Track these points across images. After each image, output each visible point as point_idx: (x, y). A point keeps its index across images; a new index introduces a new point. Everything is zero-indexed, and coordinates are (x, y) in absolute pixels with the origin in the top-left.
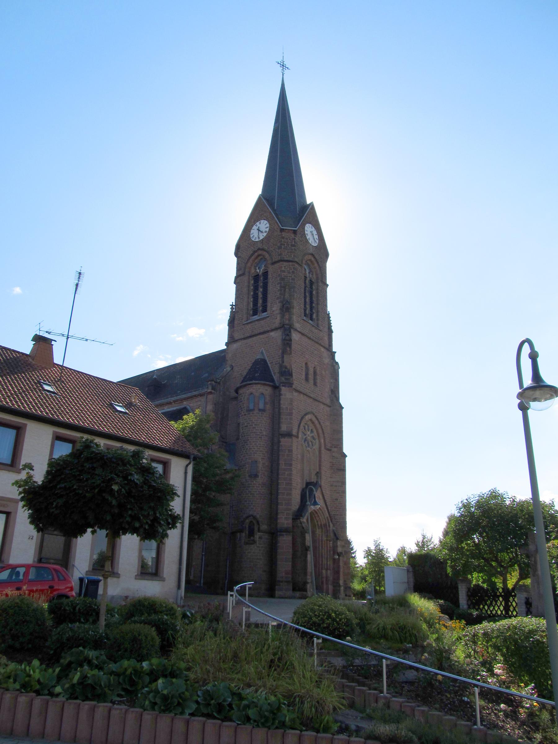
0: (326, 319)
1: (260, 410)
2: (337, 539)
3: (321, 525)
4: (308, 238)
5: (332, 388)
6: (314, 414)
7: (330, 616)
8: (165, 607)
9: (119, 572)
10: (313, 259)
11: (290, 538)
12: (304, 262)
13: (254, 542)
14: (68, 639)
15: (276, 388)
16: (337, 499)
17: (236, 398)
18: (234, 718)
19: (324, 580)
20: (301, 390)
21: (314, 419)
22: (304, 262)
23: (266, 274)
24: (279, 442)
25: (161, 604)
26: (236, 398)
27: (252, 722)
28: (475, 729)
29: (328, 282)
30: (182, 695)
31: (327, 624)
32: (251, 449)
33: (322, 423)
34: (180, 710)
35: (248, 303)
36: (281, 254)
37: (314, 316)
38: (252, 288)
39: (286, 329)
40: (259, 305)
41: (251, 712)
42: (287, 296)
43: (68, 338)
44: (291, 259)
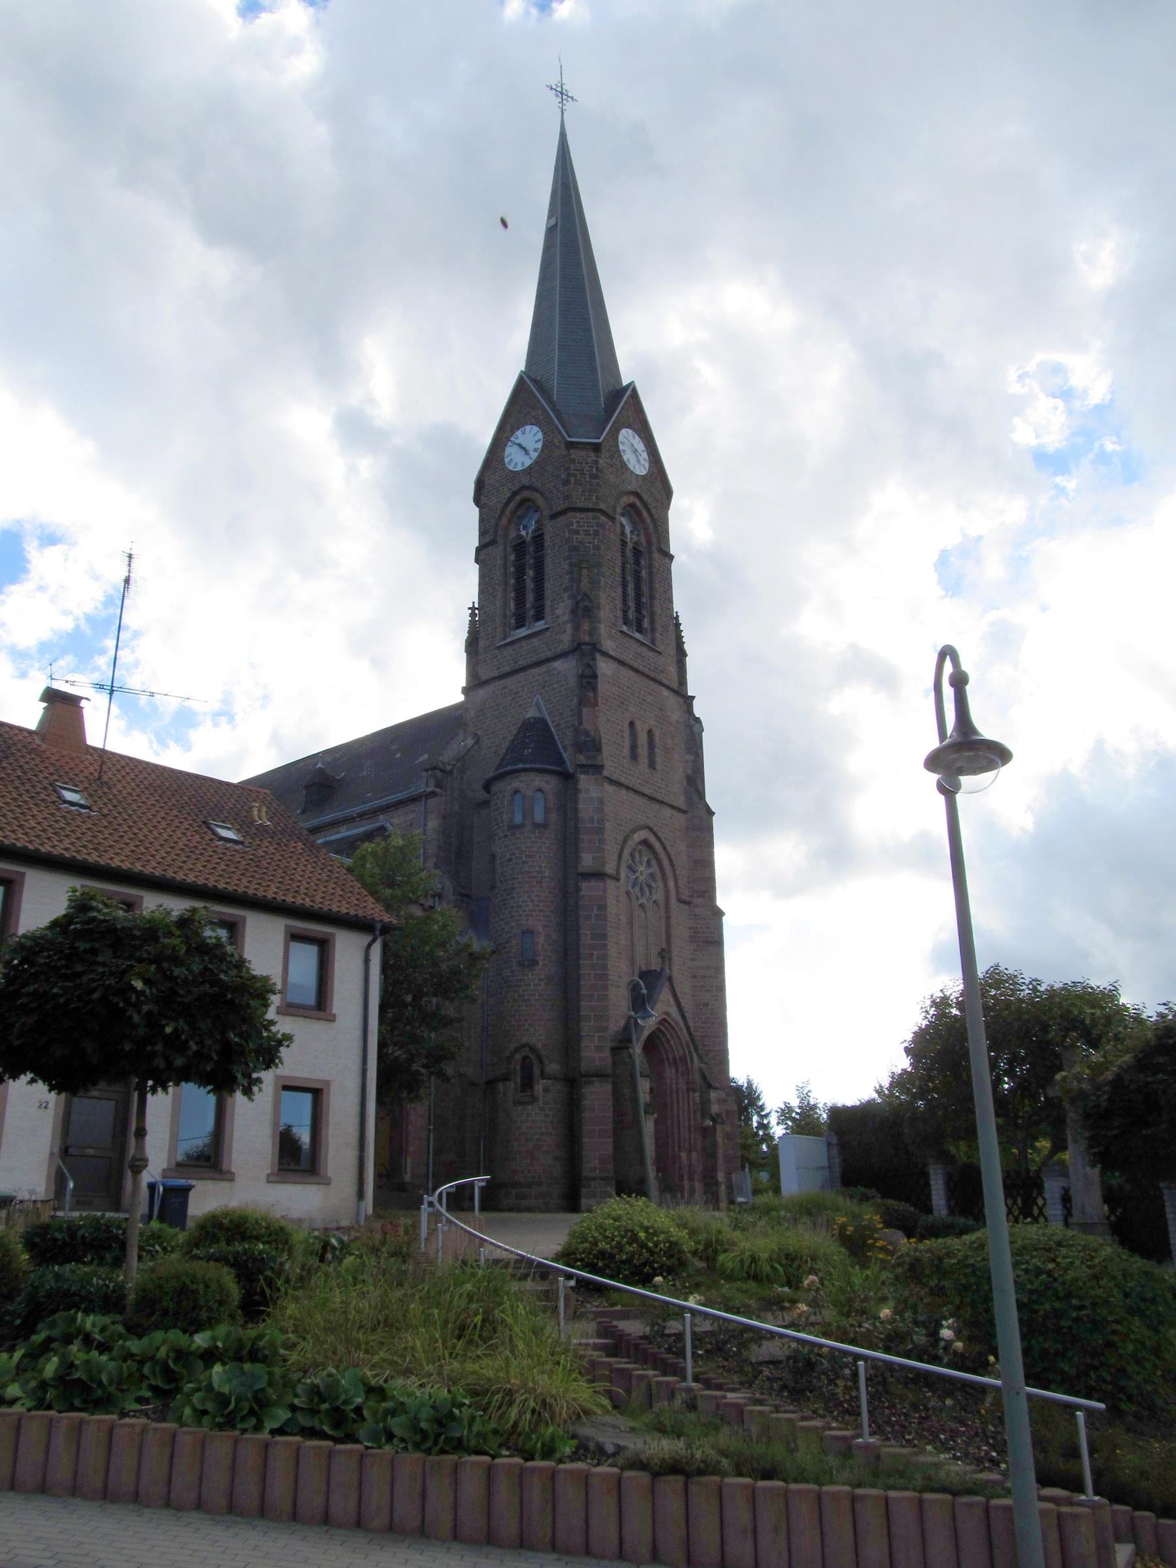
0: (672, 628)
1: (537, 826)
2: (710, 1086)
3: (674, 1058)
4: (625, 458)
5: (689, 772)
6: (651, 829)
7: (634, 1238)
8: (267, 1228)
9: (233, 1170)
10: (638, 503)
11: (608, 1088)
12: (619, 510)
13: (534, 1099)
14: (49, 1295)
15: (567, 777)
16: (707, 1005)
17: (486, 803)
18: (361, 1434)
19: (685, 1172)
20: (622, 780)
21: (652, 839)
22: (619, 510)
23: (538, 539)
24: (578, 889)
25: (257, 1222)
26: (486, 803)
27: (395, 1441)
28: (859, 1447)
29: (673, 550)
30: (260, 1395)
31: (627, 1253)
32: (519, 906)
33: (668, 848)
34: (253, 1421)
35: (505, 604)
36: (567, 497)
37: (646, 624)
38: (512, 569)
39: (586, 651)
40: (528, 605)
41: (397, 1424)
42: (585, 583)
43: (112, 692)
44: (591, 506)
